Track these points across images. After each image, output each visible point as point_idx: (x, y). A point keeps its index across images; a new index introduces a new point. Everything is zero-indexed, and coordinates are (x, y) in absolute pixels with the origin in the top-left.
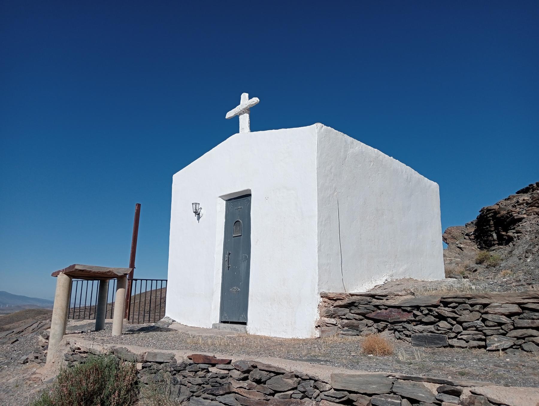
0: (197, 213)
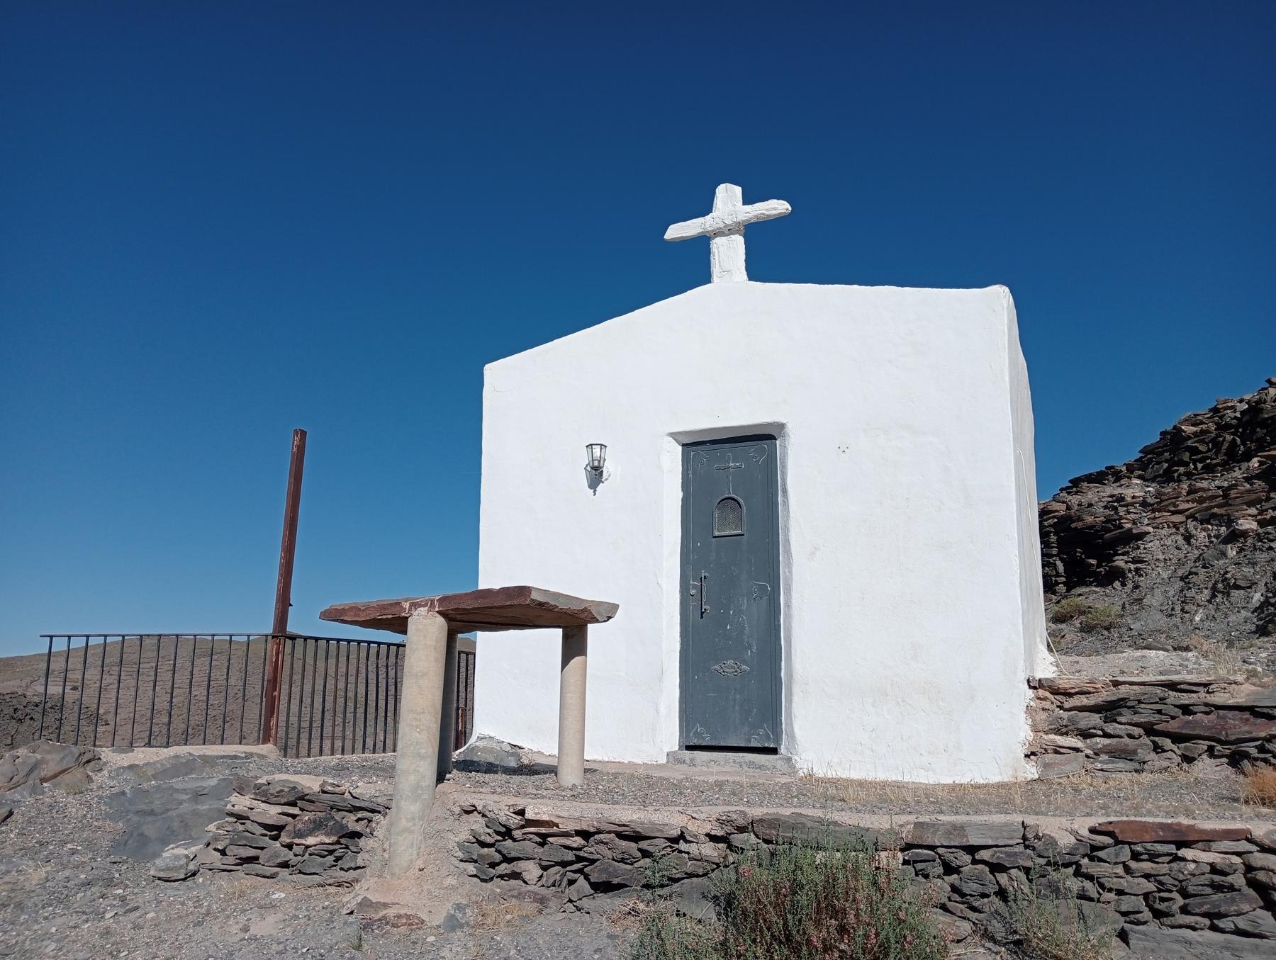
0: (596, 474)
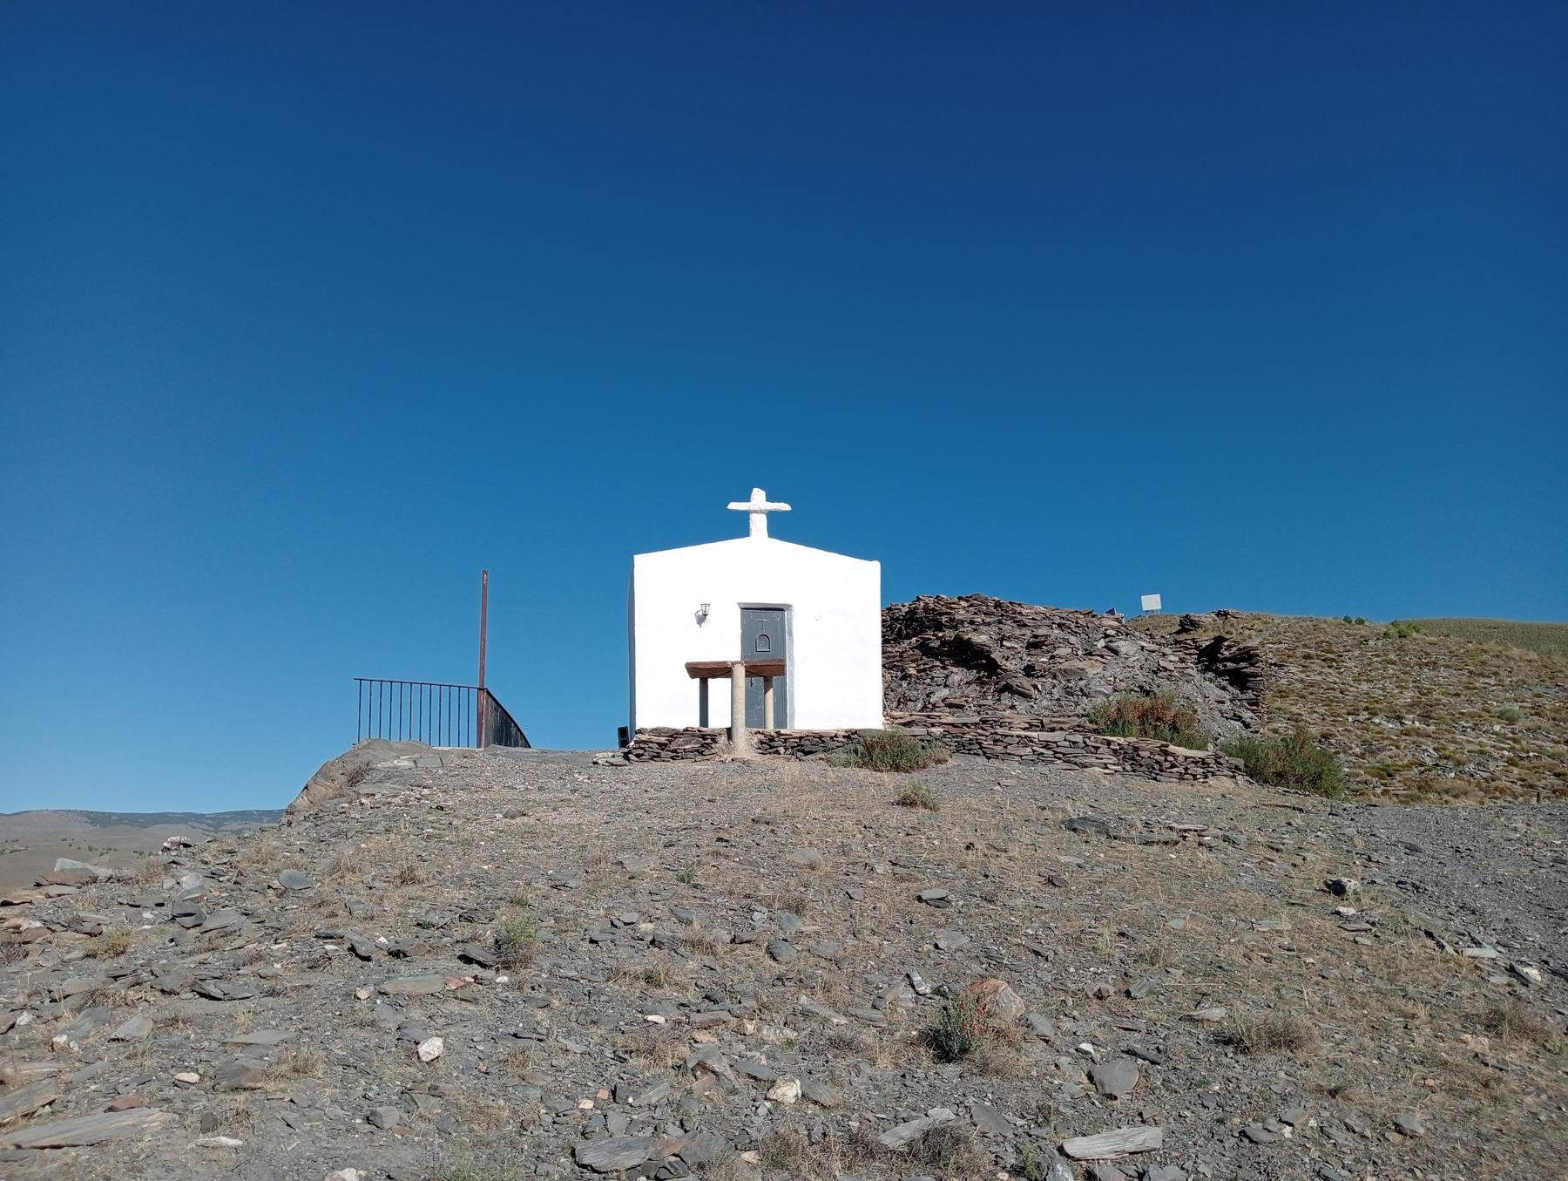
0: (702, 619)
